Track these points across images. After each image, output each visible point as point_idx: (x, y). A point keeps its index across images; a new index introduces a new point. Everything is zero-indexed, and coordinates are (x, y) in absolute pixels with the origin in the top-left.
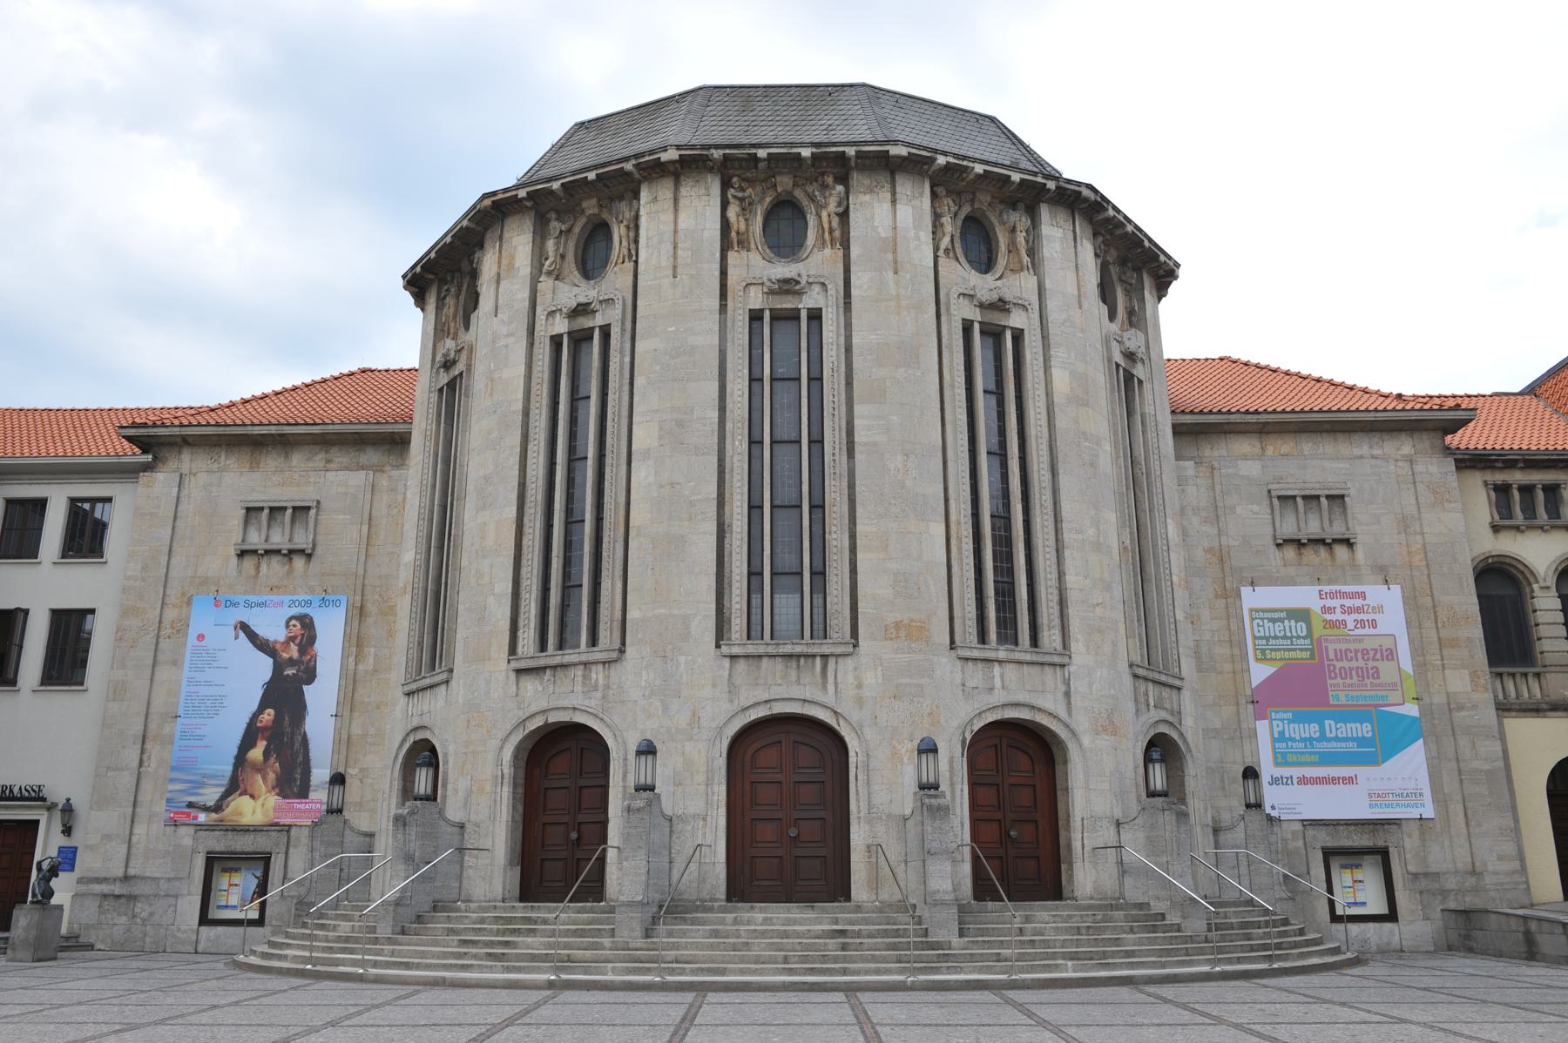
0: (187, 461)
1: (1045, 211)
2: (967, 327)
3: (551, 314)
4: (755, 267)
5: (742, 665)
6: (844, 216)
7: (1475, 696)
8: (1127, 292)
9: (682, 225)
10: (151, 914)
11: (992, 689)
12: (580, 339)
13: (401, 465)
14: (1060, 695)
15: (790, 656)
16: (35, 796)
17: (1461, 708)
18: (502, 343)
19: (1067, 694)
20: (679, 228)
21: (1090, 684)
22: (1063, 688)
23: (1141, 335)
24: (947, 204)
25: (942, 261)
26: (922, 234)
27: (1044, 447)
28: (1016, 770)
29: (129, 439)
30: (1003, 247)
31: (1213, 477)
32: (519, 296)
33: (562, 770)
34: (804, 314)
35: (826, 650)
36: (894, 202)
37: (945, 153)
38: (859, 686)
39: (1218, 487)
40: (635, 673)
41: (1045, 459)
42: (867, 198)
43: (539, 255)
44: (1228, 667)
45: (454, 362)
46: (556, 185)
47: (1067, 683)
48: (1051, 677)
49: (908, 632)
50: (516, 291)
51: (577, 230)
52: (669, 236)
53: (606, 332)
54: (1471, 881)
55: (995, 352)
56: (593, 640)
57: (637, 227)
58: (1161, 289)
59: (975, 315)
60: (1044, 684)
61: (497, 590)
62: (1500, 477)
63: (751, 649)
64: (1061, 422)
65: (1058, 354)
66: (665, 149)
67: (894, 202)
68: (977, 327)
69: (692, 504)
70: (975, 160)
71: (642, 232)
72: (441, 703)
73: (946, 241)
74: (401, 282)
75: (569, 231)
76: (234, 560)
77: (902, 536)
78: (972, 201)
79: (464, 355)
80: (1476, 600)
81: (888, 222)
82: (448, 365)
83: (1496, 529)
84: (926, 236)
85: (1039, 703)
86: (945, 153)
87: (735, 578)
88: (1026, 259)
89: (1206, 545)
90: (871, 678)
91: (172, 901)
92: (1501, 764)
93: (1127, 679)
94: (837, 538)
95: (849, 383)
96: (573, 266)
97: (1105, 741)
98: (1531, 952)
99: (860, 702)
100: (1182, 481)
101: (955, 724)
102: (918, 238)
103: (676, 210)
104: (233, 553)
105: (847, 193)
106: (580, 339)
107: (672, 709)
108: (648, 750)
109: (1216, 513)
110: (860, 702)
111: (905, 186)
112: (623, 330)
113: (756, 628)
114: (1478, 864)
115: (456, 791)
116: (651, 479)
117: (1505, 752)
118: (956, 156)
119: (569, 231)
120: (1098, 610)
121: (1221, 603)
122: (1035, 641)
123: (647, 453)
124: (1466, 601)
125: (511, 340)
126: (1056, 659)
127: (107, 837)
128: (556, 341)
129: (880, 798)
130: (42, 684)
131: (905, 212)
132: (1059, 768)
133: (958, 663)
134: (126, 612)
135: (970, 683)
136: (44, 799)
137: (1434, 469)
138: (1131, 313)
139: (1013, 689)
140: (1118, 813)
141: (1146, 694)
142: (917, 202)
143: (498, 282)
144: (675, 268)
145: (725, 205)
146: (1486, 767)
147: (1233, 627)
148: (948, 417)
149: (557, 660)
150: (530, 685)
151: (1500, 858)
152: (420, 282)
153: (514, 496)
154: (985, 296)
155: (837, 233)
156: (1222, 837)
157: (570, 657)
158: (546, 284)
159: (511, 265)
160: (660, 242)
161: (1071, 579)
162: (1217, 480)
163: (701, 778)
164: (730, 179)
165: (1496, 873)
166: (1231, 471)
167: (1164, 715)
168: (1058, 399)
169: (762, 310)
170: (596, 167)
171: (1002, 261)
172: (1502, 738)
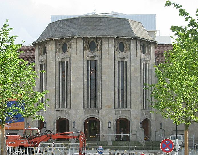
2: (119, 62)
4: (88, 53)
5: (86, 111)
6: (101, 45)
8: (148, 48)
9: (77, 47)
12: (63, 63)
18: (51, 62)
19: (131, 114)
24: (116, 42)
26: (112, 48)
27: (129, 79)
28: (123, 125)
30: (125, 47)
33: (63, 125)
34: (95, 61)
36: (108, 43)
38: (102, 114)
40: (72, 112)
41: (129, 81)
42: (104, 43)
43: (56, 48)
49: (109, 107)
50: (53, 53)
52: (76, 49)
53: (67, 62)
55: (123, 66)
56: (66, 107)
57: (71, 46)
59: (120, 60)
63: (88, 109)
66: (75, 36)
67: (108, 43)
69: (79, 89)
70: (120, 36)
71: (72, 47)
72: (44, 114)
77: (108, 93)
78: (121, 40)
79: (45, 61)
84: (113, 48)
85: (126, 115)
87: (85, 99)
93: (140, 112)
94: (99, 94)
95: (101, 71)
97: (135, 120)
99: (102, 116)
101: (114, 119)
102: (112, 49)
103: (77, 45)
107: (77, 116)
108: (74, 123)
110: (102, 116)
111: (110, 40)
112: (69, 62)
113: (88, 106)
115: (48, 126)
120: (136, 102)
122: (126, 107)
123: (73, 81)
124: (58, 142)
126: (129, 110)
128: (59, 62)
129: (104, 128)
131: (110, 45)
135: (117, 113)
138: (148, 51)
140: (137, 130)
141: (144, 113)
142: (112, 43)
143: (50, 51)
144: (77, 53)
149: (62, 110)
150: (58, 113)
154: (121, 57)
156: (156, 133)
158: (57, 53)
159: (52, 49)
163: (81, 126)
167: (147, 116)
171: (125, 49)
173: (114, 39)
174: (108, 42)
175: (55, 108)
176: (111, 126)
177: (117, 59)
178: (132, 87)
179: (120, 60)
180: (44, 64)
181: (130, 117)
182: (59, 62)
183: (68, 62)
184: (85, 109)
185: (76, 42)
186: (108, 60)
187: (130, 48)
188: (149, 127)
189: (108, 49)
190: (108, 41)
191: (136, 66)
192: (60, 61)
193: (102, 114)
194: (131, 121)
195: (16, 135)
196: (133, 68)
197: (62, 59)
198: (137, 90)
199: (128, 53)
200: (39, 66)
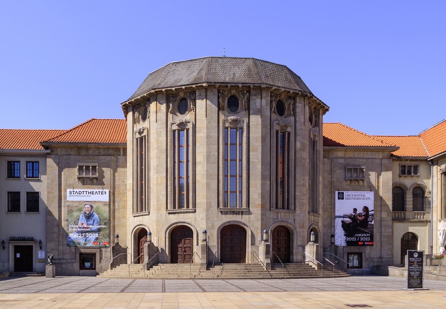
1: (298, 99)
3: (172, 124)
7: (388, 218)
10: (67, 267)
14: (293, 220)
16: (32, 239)
17: (384, 221)
19: (294, 220)
21: (299, 217)
23: (318, 128)
25: (272, 114)
26: (268, 107)
27: (293, 161)
29: (43, 146)
31: (331, 163)
32: (163, 118)
33: (180, 235)
36: (261, 98)
37: (275, 86)
39: (333, 165)
41: (293, 165)
42: (255, 97)
44: (330, 210)
45: (143, 132)
46: (173, 89)
51: (177, 100)
54: (380, 260)
58: (324, 113)
61: (162, 194)
62: (403, 163)
64: (298, 156)
65: (298, 138)
67: (261, 98)
68: (279, 131)
69: (211, 176)
73: (273, 110)
75: (176, 100)
80: (391, 195)
81: (260, 104)
83: (400, 177)
84: (268, 108)
86: (275, 86)
88: (292, 112)
89: (328, 180)
91: (72, 264)
92: (391, 234)
100: (324, 164)
102: (267, 108)
104: (76, 178)
105: (249, 95)
109: (331, 172)
114: (382, 255)
116: (201, 169)
117: (393, 231)
119: (176, 100)
121: (330, 195)
125: (161, 130)
127: (53, 249)
130: (27, 211)
131: (264, 101)
132: (291, 236)
134: (49, 193)
136: (34, 240)
137: (387, 162)
142: (267, 98)
143: (156, 113)
144: (206, 114)
145: (219, 97)
146: (388, 234)
147: (332, 201)
148: (272, 155)
151: (387, 255)
153: (165, 170)
155: (247, 107)
157: (182, 210)
160: (202, 107)
161: (297, 193)
162: (333, 164)
164: (220, 90)
165: (386, 258)
166: (336, 161)
168: (297, 149)
170: (185, 85)
171: (286, 113)
172: (392, 228)
173: (271, 93)
175: (167, 208)
178: (297, 176)
180: (145, 136)
182: (174, 131)
185: (204, 94)
187: (294, 110)
192: (175, 127)
194: (296, 231)
195: (252, 244)
196: (298, 145)
198: (304, 180)
199: (292, 119)
200: (135, 141)
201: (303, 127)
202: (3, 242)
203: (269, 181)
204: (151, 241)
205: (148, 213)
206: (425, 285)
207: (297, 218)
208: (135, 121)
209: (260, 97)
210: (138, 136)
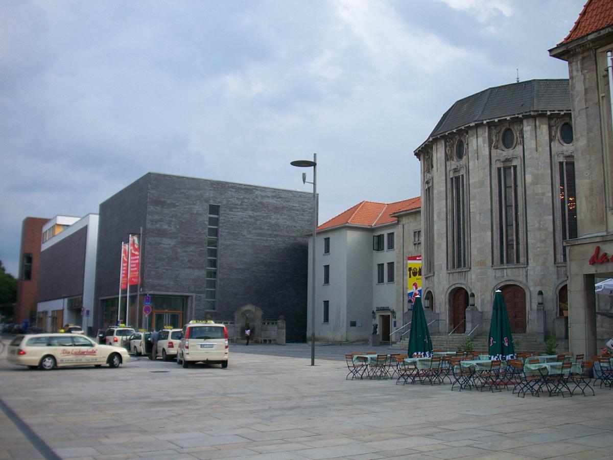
0: (404, 221)
11: (504, 276)
12: (506, 169)
13: (418, 219)
15: (459, 272)
16: (387, 309)
20: (478, 143)
22: (525, 274)
24: (494, 131)
35: (465, 270)
47: (527, 272)
48: (522, 272)
53: (515, 167)
60: (519, 273)
65: (528, 170)
70: (495, 118)
74: (414, 154)
76: (414, 246)
82: (427, 183)
84: (486, 145)
90: (473, 277)
93: (553, 269)
96: (501, 144)
98: (341, 345)
106: (506, 169)
110: (471, 283)
118: (567, 110)
131: (480, 140)
133: (494, 270)
136: (389, 310)
139: (511, 275)
142: (484, 135)
152: (418, 154)
154: (503, 159)
158: (494, 152)
168: (527, 185)
169: (501, 168)
174: (477, 135)
176: (544, 301)
177: (495, 166)
178: (528, 218)
179: (502, 166)
181: (525, 281)
182: (561, 164)
183: (518, 168)
184: (495, 268)
186: (477, 170)
188: (447, 304)
189: (477, 149)
190: (477, 132)
191: (536, 172)
193: (471, 279)
196: (529, 178)
197: (504, 162)
201: (535, 155)
202: (373, 312)
203: (490, 232)
204: (474, 305)
205: (433, 274)
206: (315, 364)
207: (530, 273)
208: (448, 158)
209: (476, 136)
210: (452, 175)
